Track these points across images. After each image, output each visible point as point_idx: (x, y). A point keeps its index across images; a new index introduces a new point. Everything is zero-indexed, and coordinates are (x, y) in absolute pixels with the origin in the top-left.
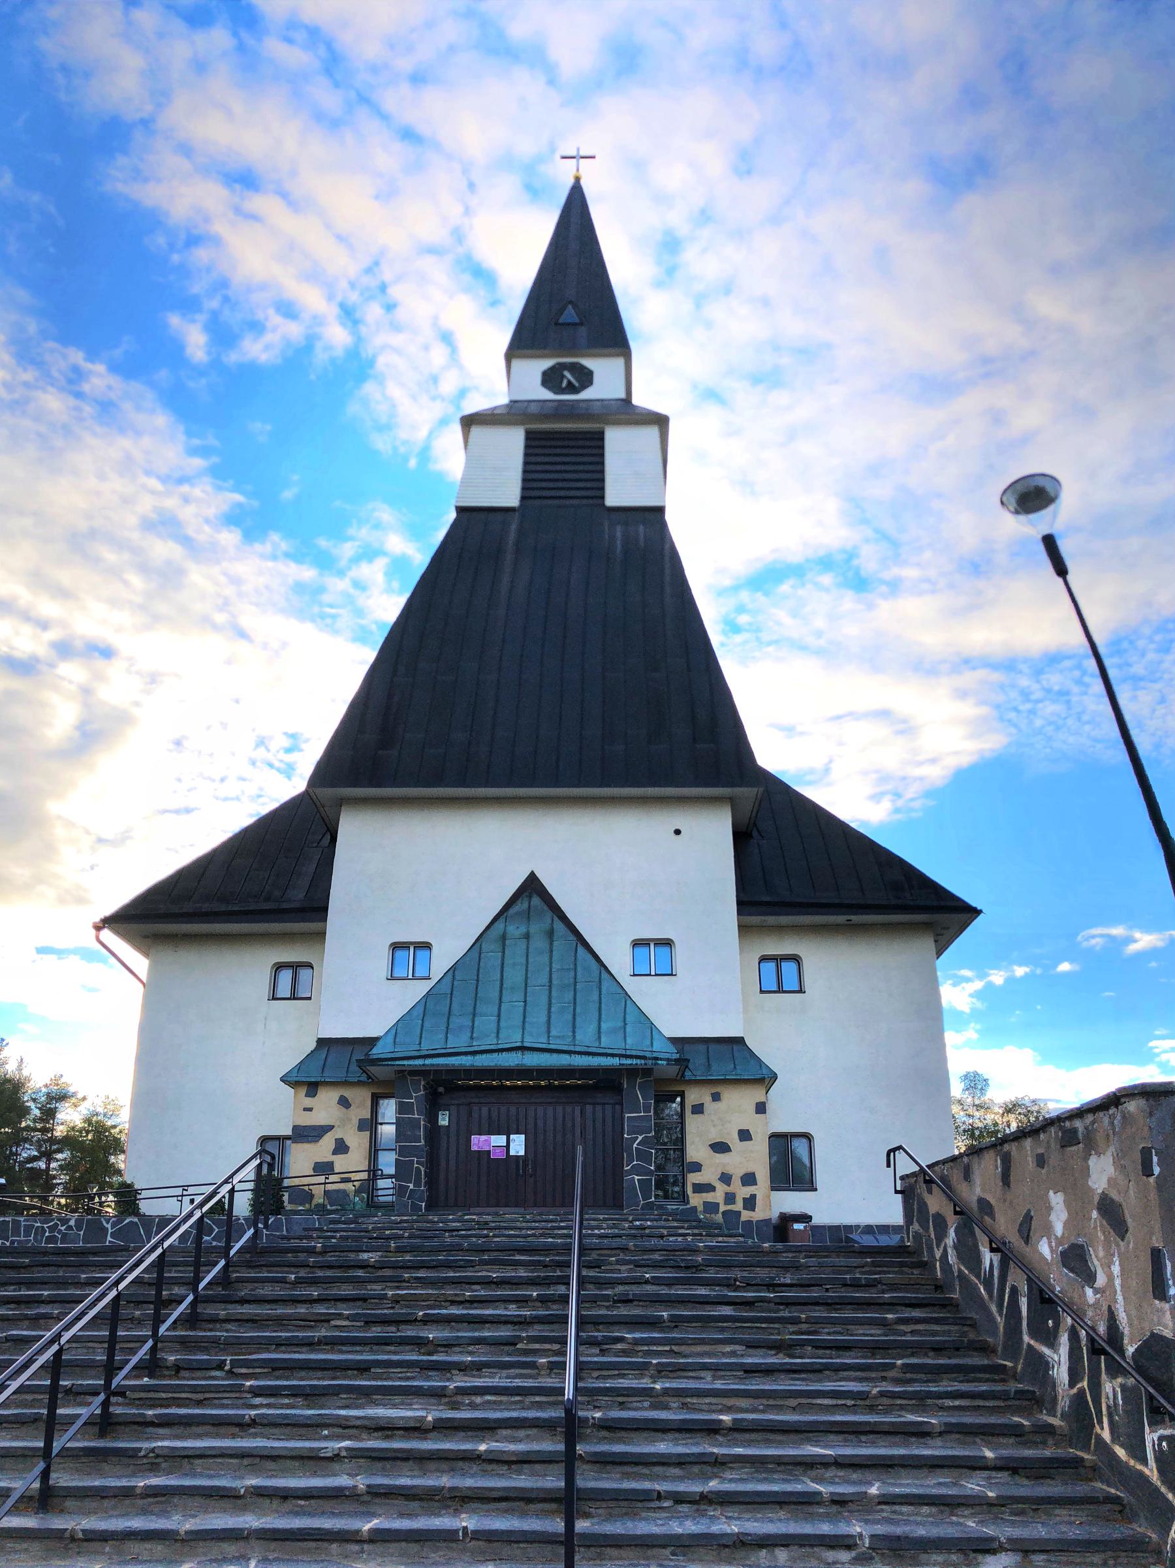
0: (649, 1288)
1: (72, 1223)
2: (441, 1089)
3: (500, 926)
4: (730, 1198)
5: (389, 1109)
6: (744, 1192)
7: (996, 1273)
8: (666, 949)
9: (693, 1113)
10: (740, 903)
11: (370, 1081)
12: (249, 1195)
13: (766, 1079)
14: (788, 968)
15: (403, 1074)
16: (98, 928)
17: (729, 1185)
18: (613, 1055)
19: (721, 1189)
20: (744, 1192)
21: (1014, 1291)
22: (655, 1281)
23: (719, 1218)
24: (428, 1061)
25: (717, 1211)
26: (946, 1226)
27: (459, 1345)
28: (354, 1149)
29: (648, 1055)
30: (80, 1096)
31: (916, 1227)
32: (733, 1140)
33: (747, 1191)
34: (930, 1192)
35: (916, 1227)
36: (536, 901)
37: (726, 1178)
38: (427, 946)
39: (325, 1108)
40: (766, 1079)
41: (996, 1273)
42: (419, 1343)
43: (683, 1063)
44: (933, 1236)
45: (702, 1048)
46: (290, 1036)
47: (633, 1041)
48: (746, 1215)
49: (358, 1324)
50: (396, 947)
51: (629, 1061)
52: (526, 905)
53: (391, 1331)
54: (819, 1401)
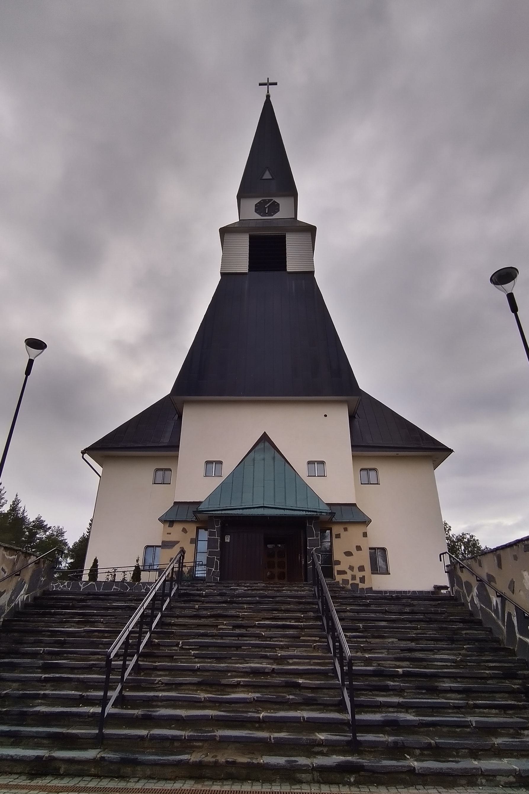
0: (349, 614)
1: (66, 584)
2: (227, 525)
3: (252, 454)
4: (354, 577)
5: (204, 535)
6: (359, 575)
7: (499, 607)
8: (322, 465)
9: (336, 538)
10: (352, 446)
11: (197, 521)
12: (132, 572)
13: (366, 522)
14: (372, 474)
15: (211, 518)
16: (83, 453)
18: (303, 511)
19: (349, 573)
20: (359, 575)
21: (509, 614)
22: (351, 611)
23: (349, 587)
24: (223, 512)
26: (472, 587)
27: (275, 637)
28: (197, 551)
29: (318, 510)
30: (48, 526)
31: (456, 588)
32: (354, 551)
33: (361, 574)
34: (462, 572)
35: (456, 588)
36: (267, 444)
37: (351, 568)
38: (221, 463)
39: (176, 533)
40: (366, 522)
41: (499, 607)
42: (259, 636)
43: (332, 514)
44: (465, 592)
45: (339, 507)
46: (163, 500)
47: (312, 506)
48: (361, 586)
49: (230, 627)
50: (207, 462)
51: (310, 513)
52: (263, 446)
53: (243, 631)
54: (436, 663)
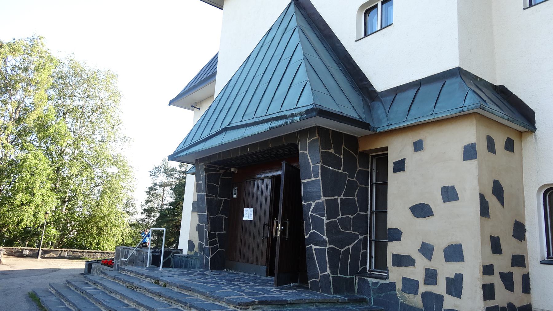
4: (431, 276)
17: (430, 258)
19: (422, 263)
23: (416, 300)
25: (416, 292)
32: (435, 201)
37: (427, 250)
51: (274, 124)
